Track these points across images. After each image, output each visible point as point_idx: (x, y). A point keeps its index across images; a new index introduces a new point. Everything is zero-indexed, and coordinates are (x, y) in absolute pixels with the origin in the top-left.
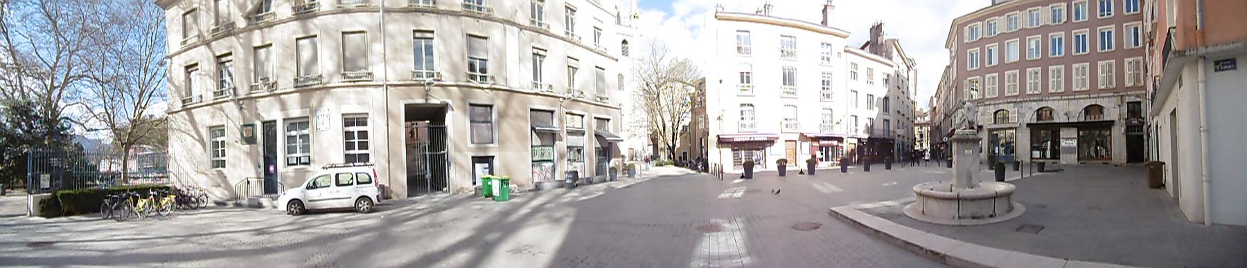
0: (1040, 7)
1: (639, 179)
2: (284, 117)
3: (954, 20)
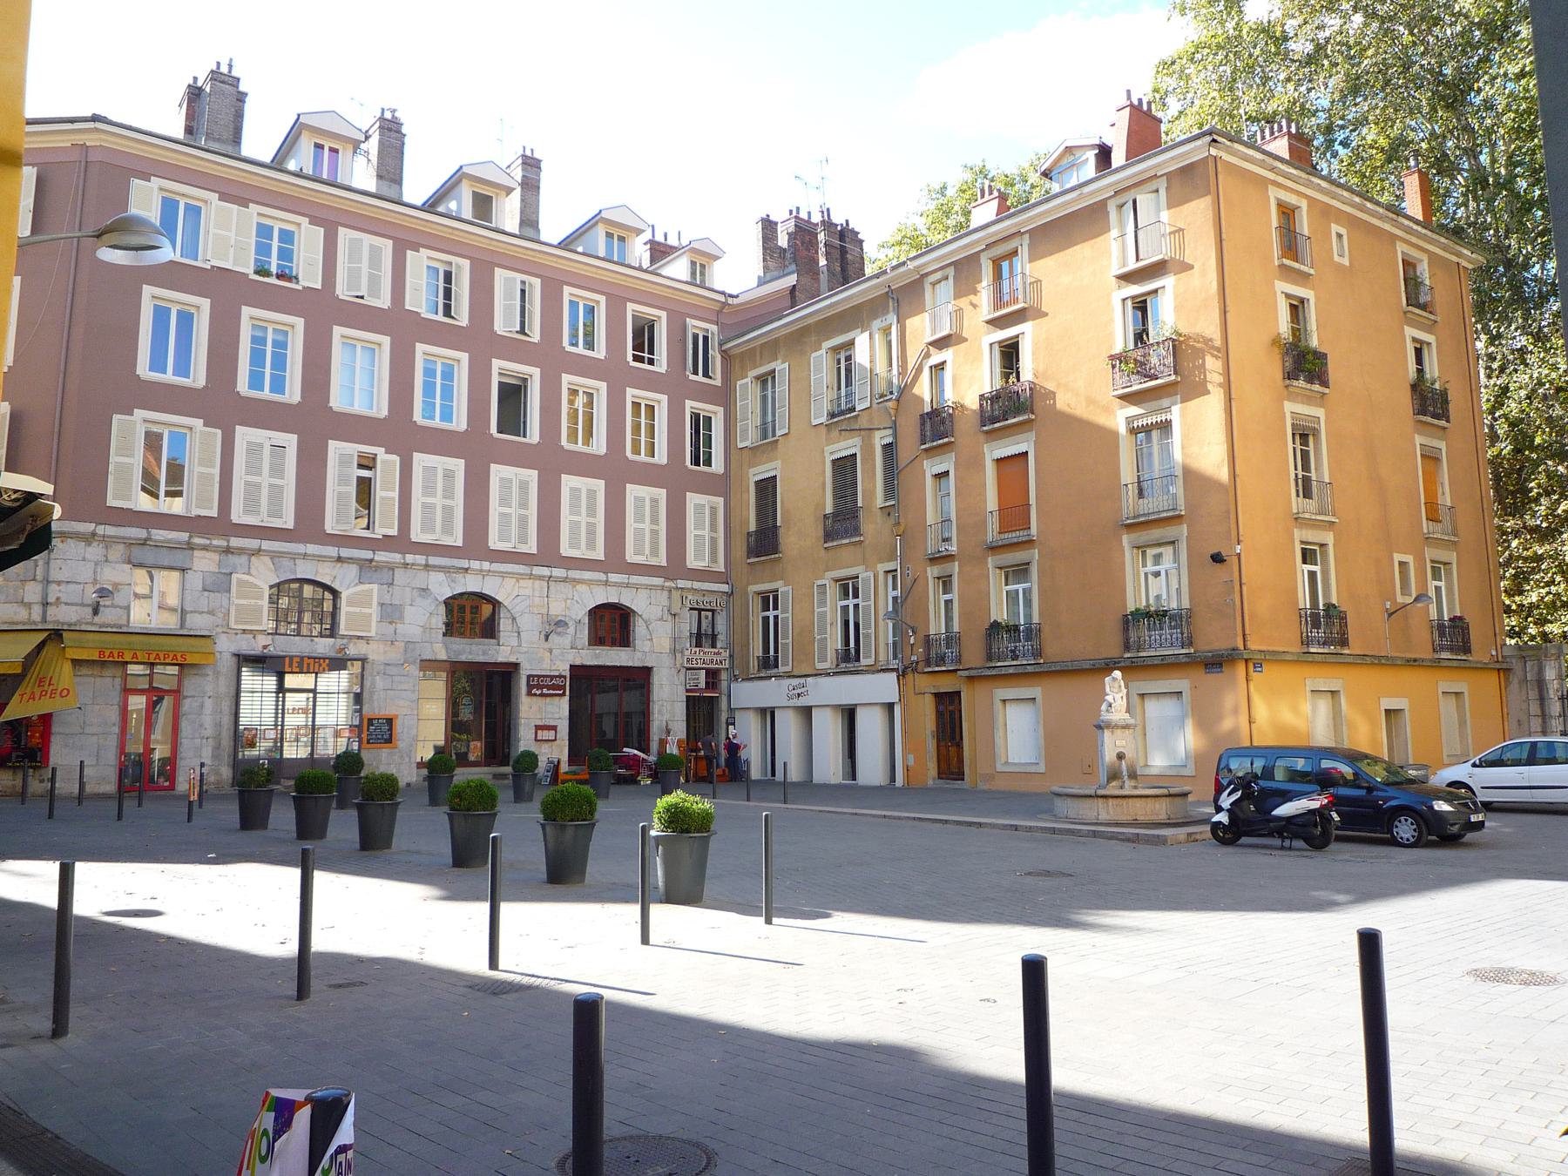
0: (304, 221)
1: (1470, 163)
2: (426, 800)
3: (95, 118)
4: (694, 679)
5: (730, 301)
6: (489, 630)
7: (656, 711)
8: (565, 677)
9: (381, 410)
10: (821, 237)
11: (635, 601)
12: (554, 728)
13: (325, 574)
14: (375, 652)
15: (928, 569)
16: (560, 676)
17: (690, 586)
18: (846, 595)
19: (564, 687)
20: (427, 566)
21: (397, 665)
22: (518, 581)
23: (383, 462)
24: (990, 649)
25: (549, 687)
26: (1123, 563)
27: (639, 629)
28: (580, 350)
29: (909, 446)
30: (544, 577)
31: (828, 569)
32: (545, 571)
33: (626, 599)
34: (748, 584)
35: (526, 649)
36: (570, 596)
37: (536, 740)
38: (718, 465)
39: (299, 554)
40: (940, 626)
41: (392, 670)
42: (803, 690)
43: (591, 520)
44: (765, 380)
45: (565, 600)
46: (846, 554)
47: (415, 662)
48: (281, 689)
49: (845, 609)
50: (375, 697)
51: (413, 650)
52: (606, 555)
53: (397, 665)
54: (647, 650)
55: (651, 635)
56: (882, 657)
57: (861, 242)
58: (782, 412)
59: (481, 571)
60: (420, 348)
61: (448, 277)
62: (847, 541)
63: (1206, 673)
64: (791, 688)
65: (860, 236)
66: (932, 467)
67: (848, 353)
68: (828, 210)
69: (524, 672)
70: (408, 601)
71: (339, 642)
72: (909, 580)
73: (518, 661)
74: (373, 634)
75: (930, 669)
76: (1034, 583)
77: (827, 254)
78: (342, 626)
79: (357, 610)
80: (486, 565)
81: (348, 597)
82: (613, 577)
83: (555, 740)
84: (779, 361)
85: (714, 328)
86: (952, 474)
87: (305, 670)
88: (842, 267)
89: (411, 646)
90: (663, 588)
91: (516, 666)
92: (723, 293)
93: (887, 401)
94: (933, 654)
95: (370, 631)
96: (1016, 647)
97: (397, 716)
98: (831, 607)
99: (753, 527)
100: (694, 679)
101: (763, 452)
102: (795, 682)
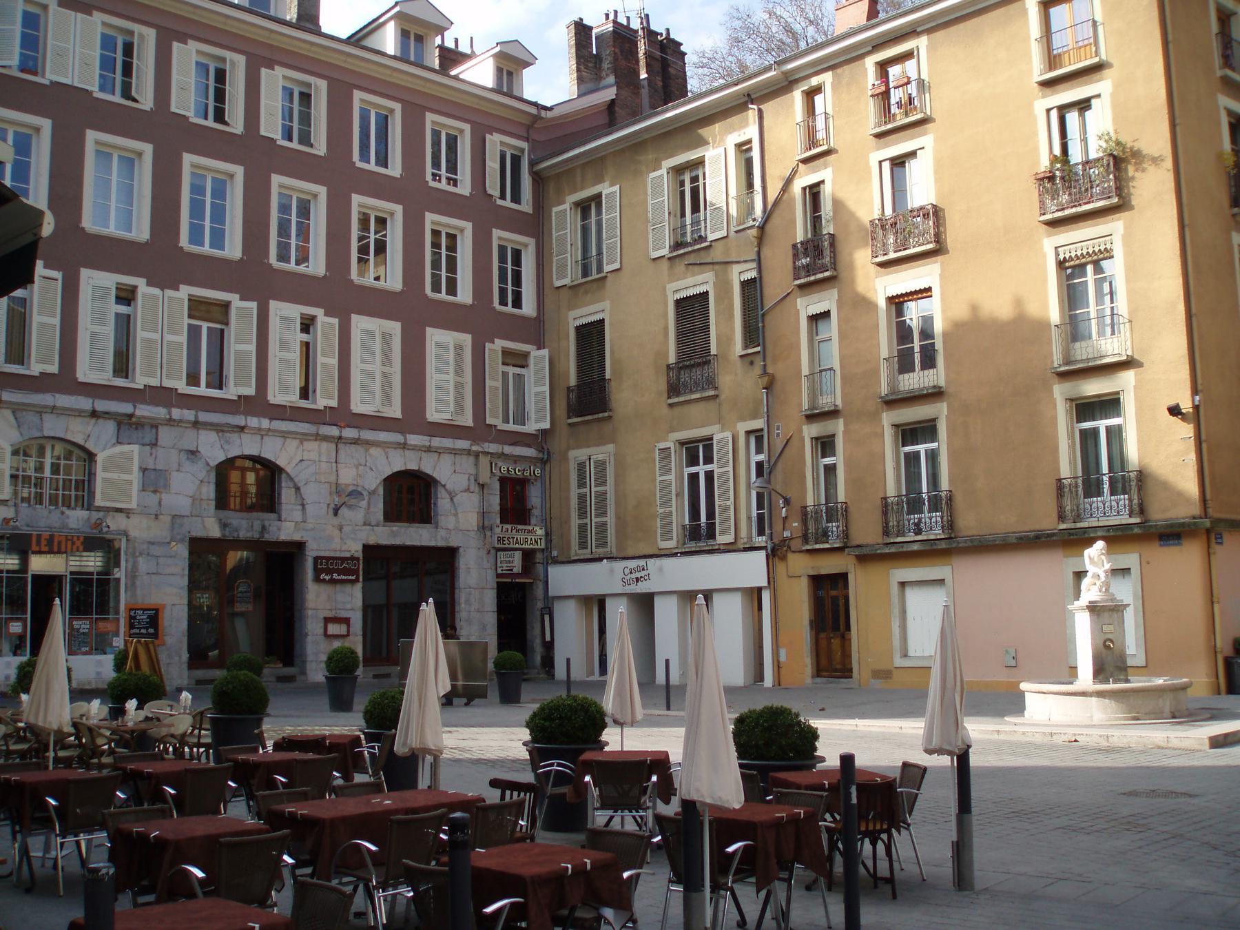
4: (509, 562)
5: (543, 113)
6: (268, 500)
7: (463, 600)
8: (358, 559)
9: (141, 231)
10: (642, 48)
11: (437, 468)
12: (346, 621)
13: (77, 431)
14: (139, 528)
15: (805, 428)
16: (353, 558)
17: (500, 451)
18: (693, 461)
19: (356, 572)
20: (196, 424)
21: (160, 544)
22: (302, 443)
23: (145, 295)
24: (887, 523)
25: (340, 572)
26: (1055, 418)
27: (443, 502)
28: (372, 166)
29: (779, 280)
30: (333, 437)
31: (672, 430)
32: (334, 431)
33: (428, 465)
34: (569, 448)
35: (310, 526)
36: (363, 462)
37: (326, 635)
38: (529, 308)
39: (46, 407)
40: (819, 495)
41: (156, 550)
42: (642, 574)
43: (387, 369)
44: (584, 207)
45: (357, 468)
46: (695, 411)
47: (181, 541)
48: (67, 561)
49: (694, 478)
50: (138, 583)
51: (181, 525)
52: (403, 411)
53: (160, 544)
54: (451, 526)
55: (456, 509)
56: (743, 533)
57: (684, 54)
58: (611, 241)
59: (260, 429)
60: (188, 159)
61: (221, 76)
62: (697, 396)
63: (1161, 545)
64: (627, 571)
65: (682, 48)
66: (809, 305)
67: (694, 174)
68: (647, 16)
69: (312, 551)
70: (175, 466)
71: (96, 515)
72: (779, 445)
73: (304, 539)
74: (134, 505)
75: (809, 547)
76: (942, 444)
77: (648, 65)
78: (98, 495)
79: (115, 476)
80: (265, 423)
81: (104, 461)
82: (414, 439)
83: (348, 635)
84: (607, 184)
85: (524, 145)
86: (834, 315)
87: (56, 549)
88: (663, 81)
89: (178, 521)
90: (469, 452)
91: (300, 546)
92: (535, 104)
93: (749, 228)
94: (812, 529)
95: (130, 502)
96: (920, 519)
97: (164, 606)
98: (676, 475)
99: (573, 381)
100: (509, 562)
101: (586, 292)
102: (632, 564)
